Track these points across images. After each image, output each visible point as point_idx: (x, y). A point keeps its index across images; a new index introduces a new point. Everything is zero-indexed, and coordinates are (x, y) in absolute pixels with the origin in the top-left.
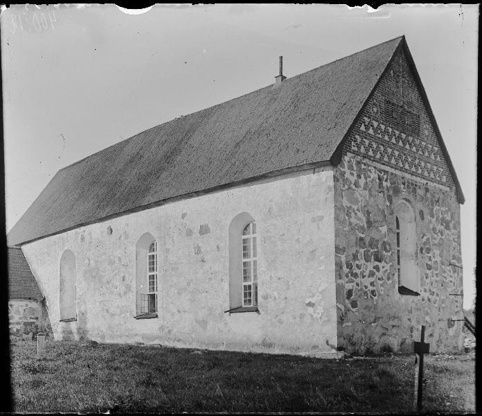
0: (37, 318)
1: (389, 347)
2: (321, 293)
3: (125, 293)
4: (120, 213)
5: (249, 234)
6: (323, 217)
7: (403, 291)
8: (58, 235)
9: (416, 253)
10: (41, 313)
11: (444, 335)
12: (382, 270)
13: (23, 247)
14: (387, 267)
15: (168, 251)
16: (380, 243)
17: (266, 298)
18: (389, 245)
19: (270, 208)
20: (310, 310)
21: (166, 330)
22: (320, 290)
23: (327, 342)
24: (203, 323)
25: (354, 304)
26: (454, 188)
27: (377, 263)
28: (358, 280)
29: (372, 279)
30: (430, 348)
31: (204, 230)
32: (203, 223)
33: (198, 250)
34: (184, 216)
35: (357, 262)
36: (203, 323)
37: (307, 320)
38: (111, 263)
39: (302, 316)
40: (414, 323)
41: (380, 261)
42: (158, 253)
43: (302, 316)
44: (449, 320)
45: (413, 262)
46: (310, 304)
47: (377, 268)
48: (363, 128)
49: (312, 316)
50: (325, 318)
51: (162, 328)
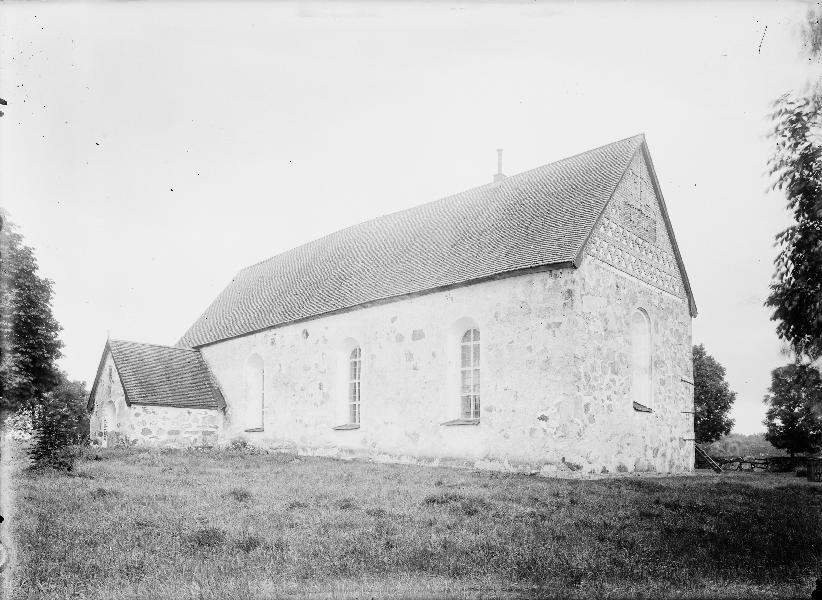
0: (217, 428)
1: (624, 467)
2: (556, 405)
3: (322, 402)
4: (689, 301)
5: (469, 341)
6: (560, 323)
7: (638, 408)
8: (242, 339)
9: (651, 368)
10: (222, 422)
11: (676, 456)
12: (618, 383)
13: (204, 351)
14: (623, 380)
15: (373, 357)
16: (617, 354)
17: (489, 410)
18: (626, 358)
19: (496, 313)
20: (543, 424)
21: (369, 443)
22: (555, 402)
23: (564, 459)
24: (415, 437)
25: (592, 420)
26: (687, 300)
27: (614, 376)
28: (596, 393)
29: (610, 393)
30: (661, 468)
31: (417, 335)
32: (425, 331)
33: (410, 356)
34: (393, 320)
35: (595, 373)
36: (415, 437)
37: (539, 434)
38: (307, 369)
39: (532, 431)
40: (648, 442)
41: (616, 374)
42: (363, 358)
43: (532, 431)
44: (680, 439)
45: (647, 375)
46: (543, 418)
47: (613, 381)
48: (602, 229)
49: (545, 431)
50: (559, 433)
51: (364, 441)
